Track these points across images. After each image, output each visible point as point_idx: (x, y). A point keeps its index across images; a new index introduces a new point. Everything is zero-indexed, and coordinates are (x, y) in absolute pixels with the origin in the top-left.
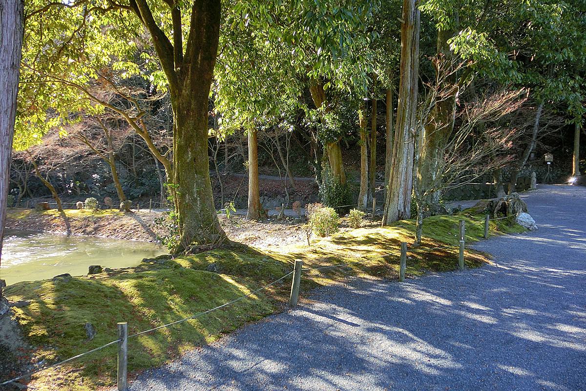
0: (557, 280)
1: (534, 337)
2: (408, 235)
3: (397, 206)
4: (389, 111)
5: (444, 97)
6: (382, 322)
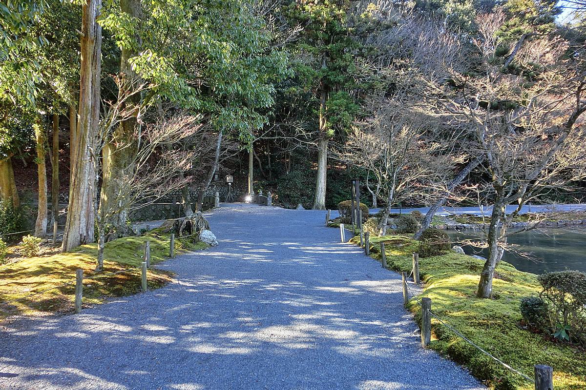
0: (229, 290)
1: (207, 349)
2: (90, 260)
3: (78, 230)
4: (73, 128)
5: (125, 117)
6: (49, 365)
